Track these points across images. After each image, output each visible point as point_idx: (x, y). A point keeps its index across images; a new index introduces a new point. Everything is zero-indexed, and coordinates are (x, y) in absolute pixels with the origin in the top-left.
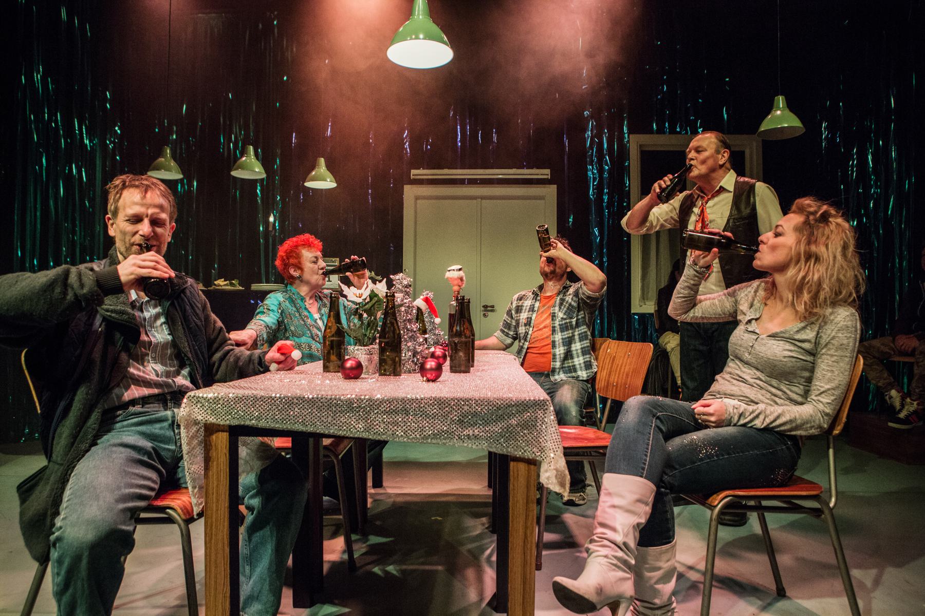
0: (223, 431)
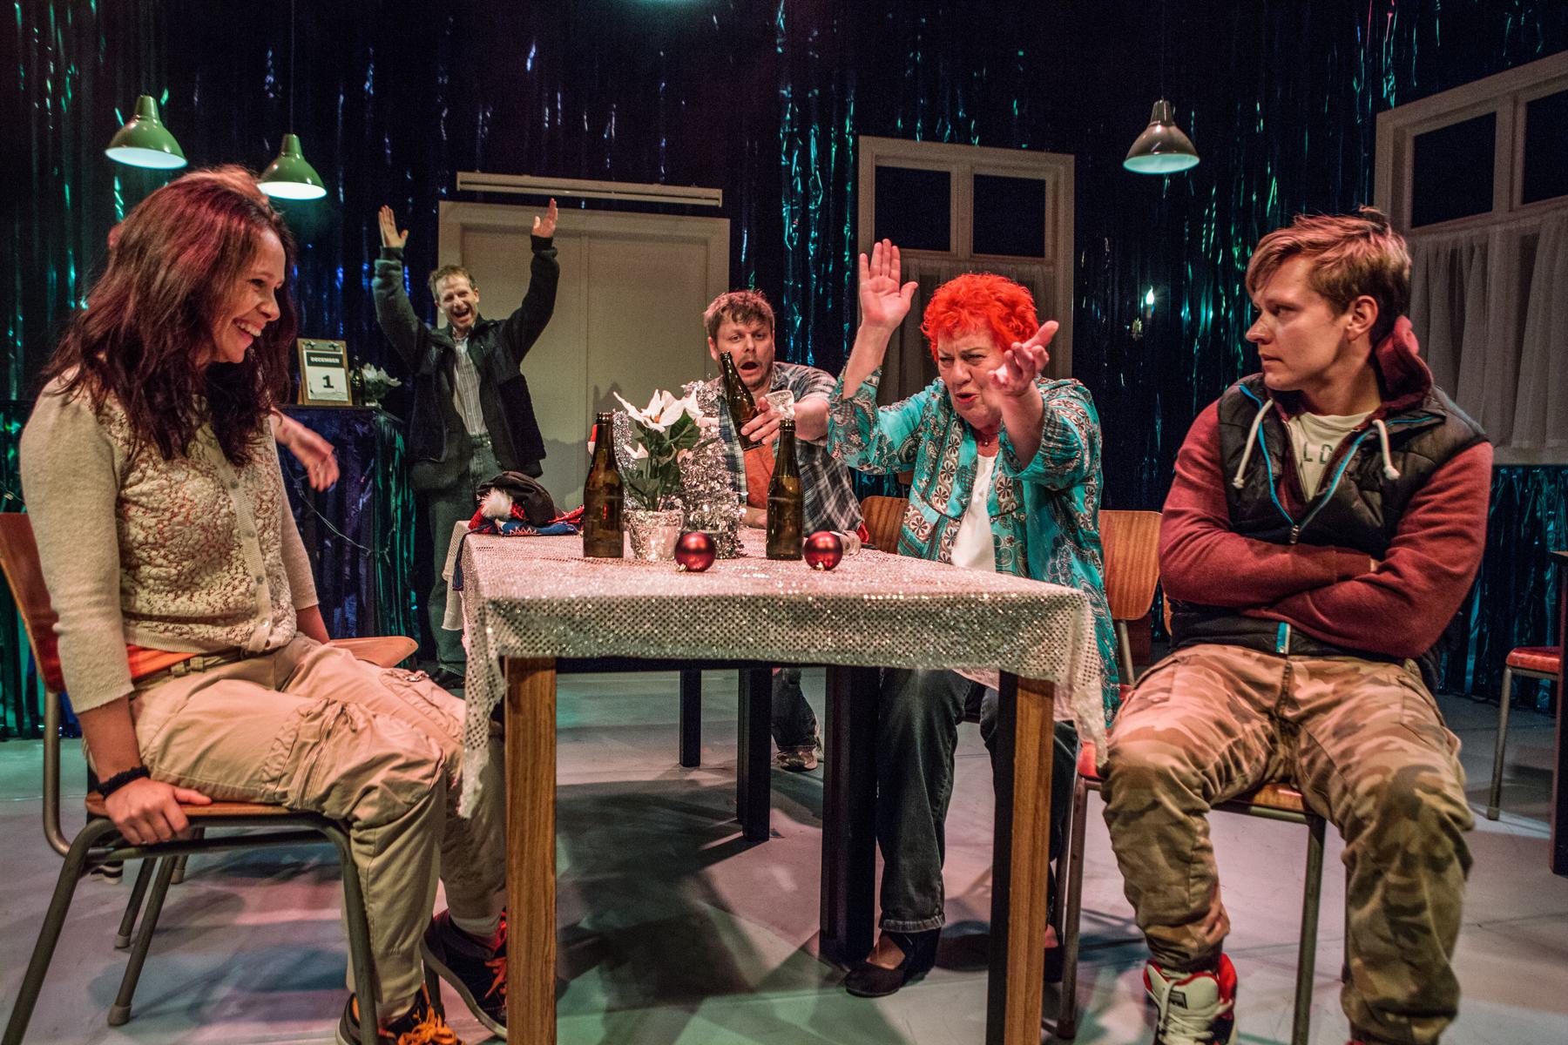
0: (545, 669)
